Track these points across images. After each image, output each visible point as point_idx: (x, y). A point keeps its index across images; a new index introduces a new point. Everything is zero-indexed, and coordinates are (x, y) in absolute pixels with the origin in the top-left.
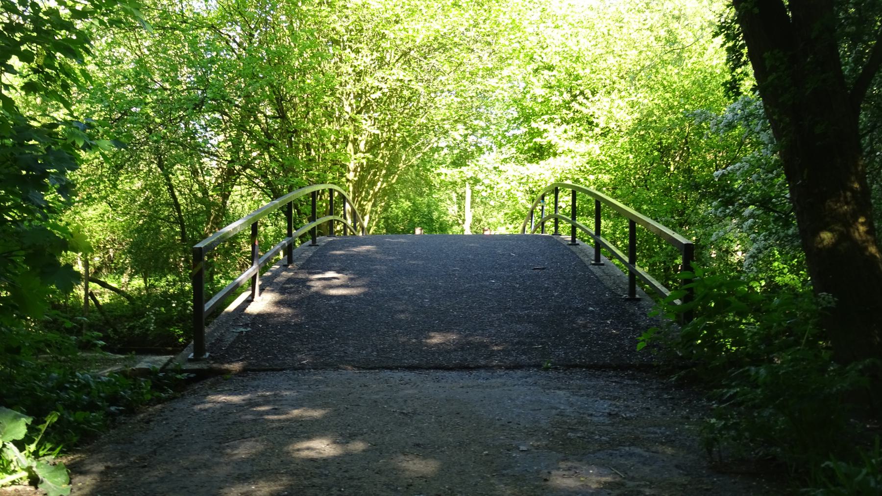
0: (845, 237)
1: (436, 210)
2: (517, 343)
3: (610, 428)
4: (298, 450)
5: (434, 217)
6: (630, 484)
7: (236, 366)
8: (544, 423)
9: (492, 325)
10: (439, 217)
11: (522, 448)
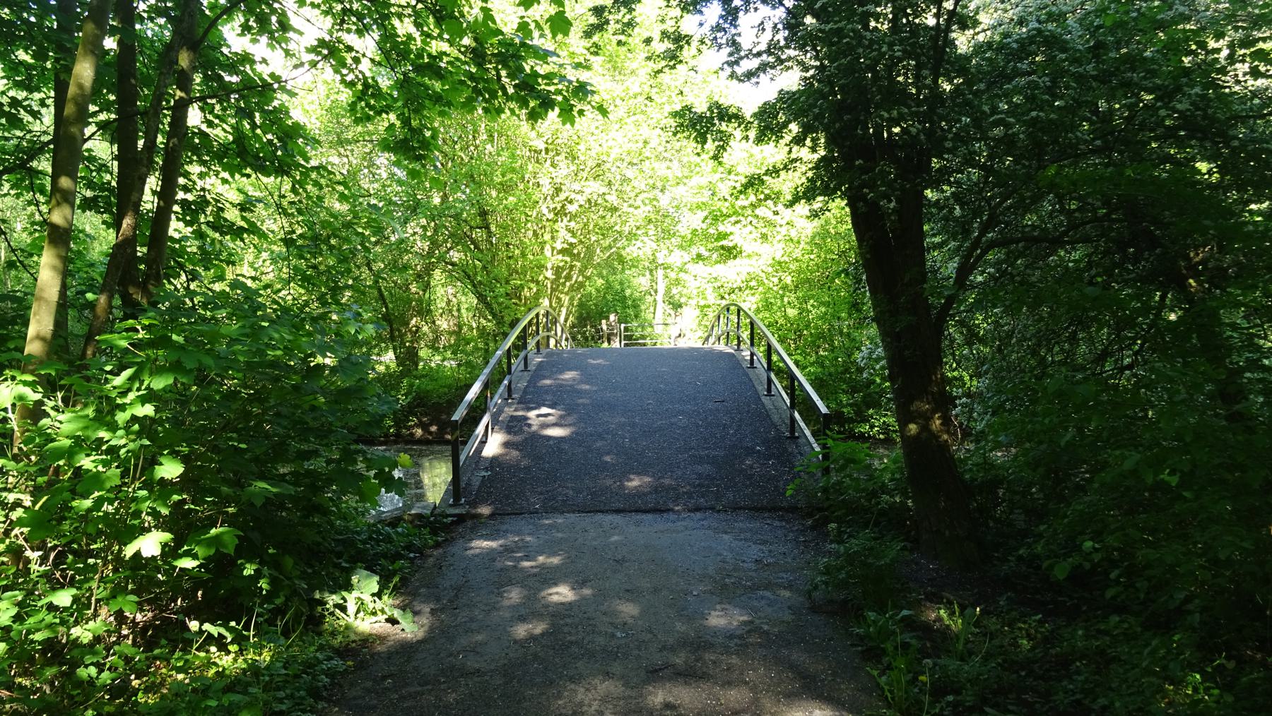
0: (925, 428)
1: (629, 287)
2: (698, 485)
3: (754, 574)
4: (551, 594)
5: (627, 295)
6: (757, 621)
7: (485, 510)
8: (711, 571)
9: (678, 467)
10: (632, 294)
11: (695, 593)
